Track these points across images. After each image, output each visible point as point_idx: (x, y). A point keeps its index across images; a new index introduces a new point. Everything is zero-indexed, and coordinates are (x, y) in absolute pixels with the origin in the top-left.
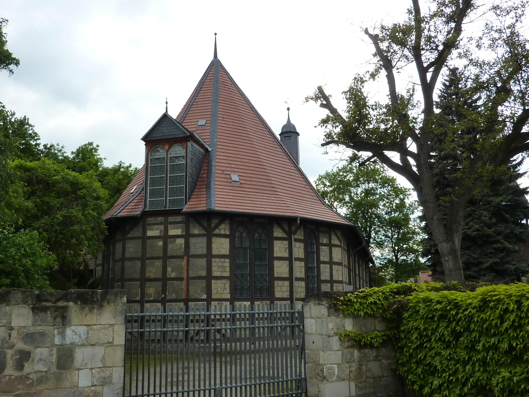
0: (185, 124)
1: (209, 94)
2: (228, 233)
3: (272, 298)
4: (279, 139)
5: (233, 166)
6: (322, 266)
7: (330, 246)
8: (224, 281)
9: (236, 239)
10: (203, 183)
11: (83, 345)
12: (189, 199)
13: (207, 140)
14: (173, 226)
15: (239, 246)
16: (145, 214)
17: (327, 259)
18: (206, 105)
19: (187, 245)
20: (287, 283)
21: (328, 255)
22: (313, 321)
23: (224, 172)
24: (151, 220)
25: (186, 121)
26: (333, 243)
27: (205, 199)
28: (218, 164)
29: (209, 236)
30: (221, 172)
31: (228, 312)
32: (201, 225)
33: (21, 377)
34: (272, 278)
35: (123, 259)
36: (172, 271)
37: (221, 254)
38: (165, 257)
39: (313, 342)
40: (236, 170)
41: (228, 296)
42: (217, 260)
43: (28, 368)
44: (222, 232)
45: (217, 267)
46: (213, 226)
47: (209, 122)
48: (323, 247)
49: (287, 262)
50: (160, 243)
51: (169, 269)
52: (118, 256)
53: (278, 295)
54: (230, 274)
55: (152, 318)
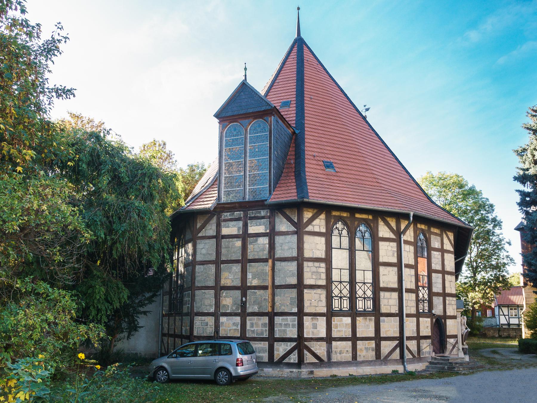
8: (319, 291)
12: (276, 183)
14: (254, 221)
16: (220, 208)
17: (439, 268)
20: (395, 295)
21: (441, 263)
23: (316, 158)
24: (227, 215)
30: (312, 158)
36: (254, 278)
37: (314, 257)
38: (244, 261)
42: (310, 264)
44: (317, 229)
49: (396, 269)
51: (249, 276)
54: (327, 282)
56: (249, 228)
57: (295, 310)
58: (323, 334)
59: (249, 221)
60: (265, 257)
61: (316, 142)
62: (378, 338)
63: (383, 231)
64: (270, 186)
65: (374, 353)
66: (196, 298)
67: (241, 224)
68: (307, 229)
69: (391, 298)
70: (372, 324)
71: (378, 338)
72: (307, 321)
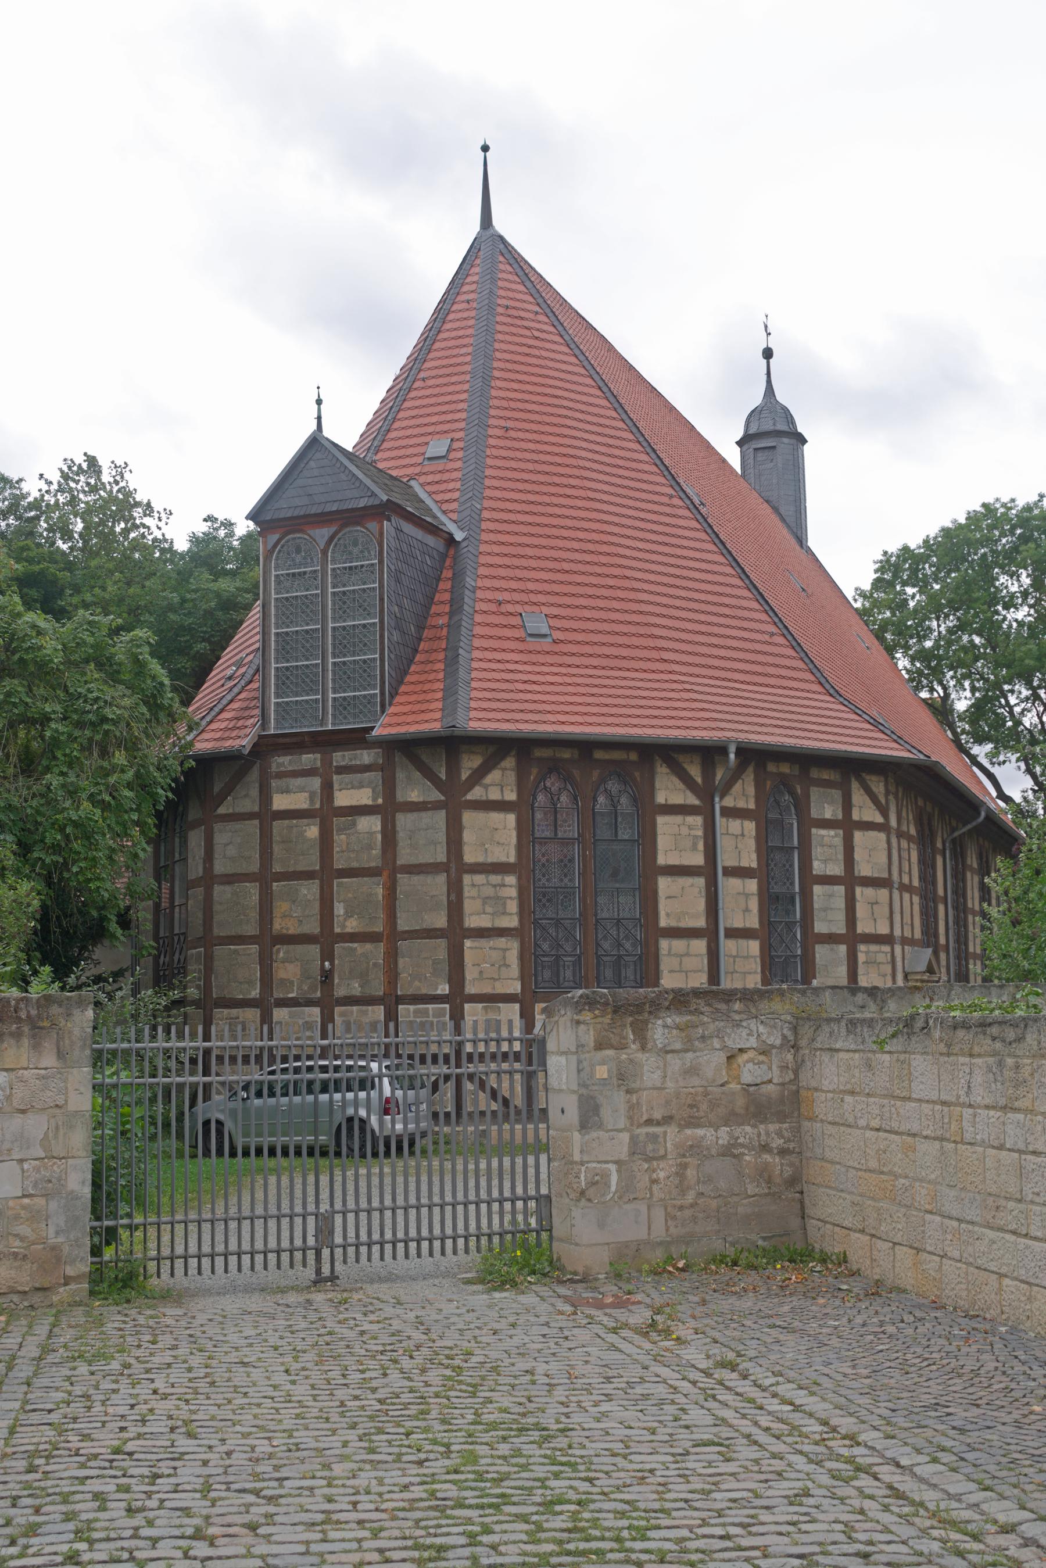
1: (463, 351)
2: (511, 796)
5: (531, 586)
6: (817, 889)
7: (848, 826)
8: (502, 942)
9: (539, 816)
10: (435, 645)
13: (454, 506)
14: (347, 778)
15: (548, 834)
16: (266, 747)
18: (451, 389)
20: (700, 946)
21: (841, 857)
22: (563, 1060)
23: (504, 608)
24: (283, 762)
26: (856, 816)
27: (440, 695)
28: (483, 582)
29: (453, 806)
30: (493, 607)
31: (517, 1034)
32: (430, 775)
34: (650, 930)
35: (209, 879)
36: (348, 915)
38: (327, 874)
40: (541, 598)
41: (516, 987)
42: (479, 879)
44: (494, 795)
45: (479, 902)
46: (465, 775)
47: (461, 444)
50: (313, 832)
51: (339, 909)
52: (196, 869)
55: (294, 1052)
56: (337, 795)
59: (335, 777)
60: (373, 864)
61: (507, 561)
63: (667, 788)
64: (382, 693)
66: (216, 963)
67: (316, 783)
68: (469, 797)
69: (687, 954)
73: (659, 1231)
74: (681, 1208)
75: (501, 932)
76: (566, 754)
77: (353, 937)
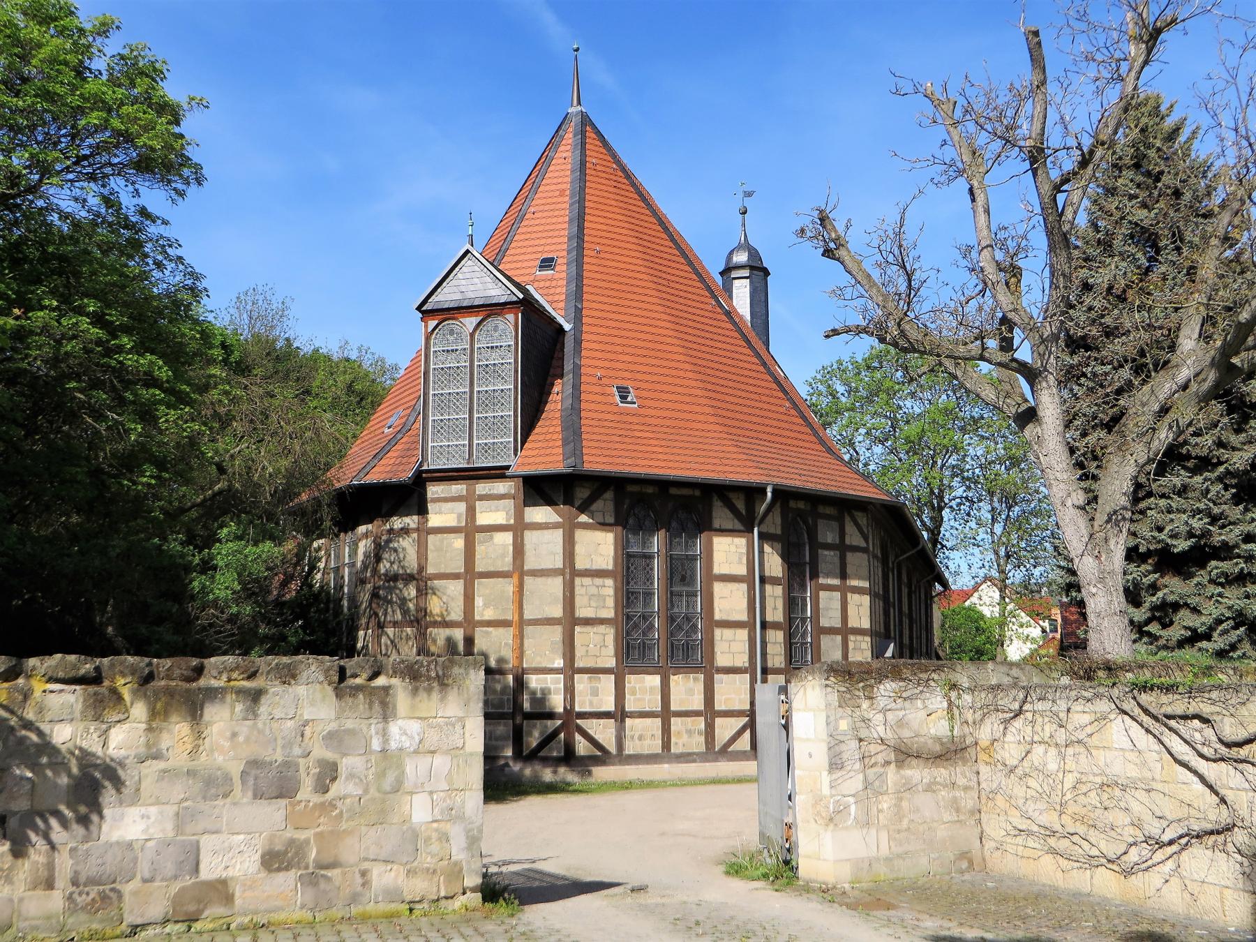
0: (508, 266)
3: (709, 670)
4: (720, 283)
8: (602, 629)
11: (416, 752)
12: (523, 444)
19: (519, 550)
24: (433, 490)
25: (510, 259)
33: (323, 804)
37: (594, 567)
39: (810, 756)
41: (611, 663)
42: (587, 581)
43: (335, 789)
48: (826, 553)
49: (744, 587)
51: (479, 602)
53: (722, 660)
57: (559, 663)
58: (610, 706)
62: (710, 712)
65: (702, 739)
70: (699, 687)
71: (710, 712)
72: (581, 682)
73: (884, 851)
74: (899, 832)
75: (602, 621)
76: (650, 490)
77: (489, 623)
